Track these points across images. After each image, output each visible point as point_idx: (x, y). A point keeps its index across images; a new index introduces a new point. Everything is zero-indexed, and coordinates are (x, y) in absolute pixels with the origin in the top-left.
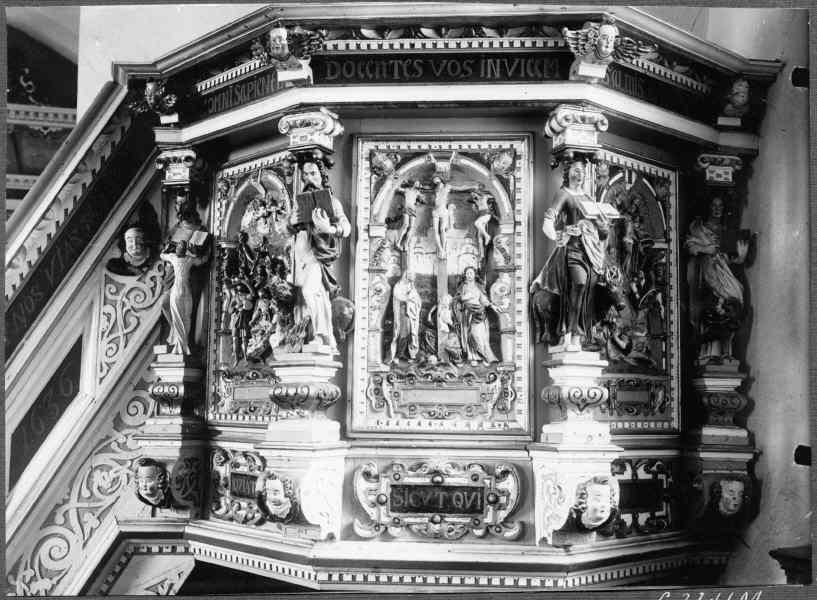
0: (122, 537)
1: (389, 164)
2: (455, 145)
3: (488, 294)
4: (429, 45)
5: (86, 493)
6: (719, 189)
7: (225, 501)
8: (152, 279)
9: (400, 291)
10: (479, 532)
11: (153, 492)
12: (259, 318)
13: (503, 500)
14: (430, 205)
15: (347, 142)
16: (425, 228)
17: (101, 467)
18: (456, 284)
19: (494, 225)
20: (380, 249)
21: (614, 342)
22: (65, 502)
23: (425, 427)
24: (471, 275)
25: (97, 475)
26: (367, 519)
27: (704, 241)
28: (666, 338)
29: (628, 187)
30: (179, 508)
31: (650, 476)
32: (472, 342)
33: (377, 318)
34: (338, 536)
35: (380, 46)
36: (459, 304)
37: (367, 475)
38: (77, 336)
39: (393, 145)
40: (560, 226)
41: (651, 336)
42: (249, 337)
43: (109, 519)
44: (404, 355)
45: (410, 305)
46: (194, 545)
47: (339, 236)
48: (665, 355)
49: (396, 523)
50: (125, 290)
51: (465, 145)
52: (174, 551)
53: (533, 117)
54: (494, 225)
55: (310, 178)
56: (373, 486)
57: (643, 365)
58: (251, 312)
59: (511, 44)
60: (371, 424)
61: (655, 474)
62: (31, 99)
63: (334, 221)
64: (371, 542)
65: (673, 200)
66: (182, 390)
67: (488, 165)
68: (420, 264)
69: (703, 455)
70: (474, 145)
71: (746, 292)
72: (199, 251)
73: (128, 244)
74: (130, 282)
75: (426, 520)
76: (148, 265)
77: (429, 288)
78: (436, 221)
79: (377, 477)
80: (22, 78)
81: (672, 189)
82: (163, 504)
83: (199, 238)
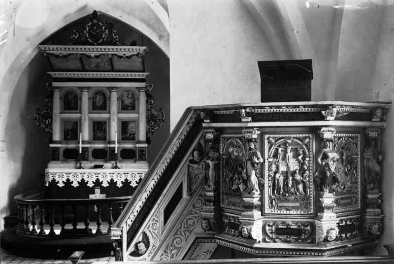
0: (197, 238)
1: (273, 141)
2: (292, 136)
3: (302, 177)
4: (284, 110)
5: (186, 226)
6: (375, 139)
7: (227, 229)
8: (202, 165)
9: (277, 176)
10: (300, 241)
11: (207, 227)
12: (236, 179)
13: (307, 232)
14: (285, 152)
15: (261, 136)
16: (284, 158)
17: (190, 219)
18: (294, 173)
19: (304, 159)
20: (271, 164)
21: (340, 187)
22: (180, 228)
23: (285, 212)
24: (297, 171)
25: (189, 221)
26: (269, 237)
27: (369, 154)
28: (356, 183)
29: (344, 142)
30: (214, 231)
31: (351, 223)
32: (298, 189)
33: (271, 183)
34: (261, 241)
35: (270, 111)
36: (294, 180)
37: (269, 226)
38: (180, 183)
39: (274, 135)
40: (322, 159)
41: (352, 183)
42: (233, 184)
43: (193, 233)
44: (279, 193)
45: (280, 180)
46: (217, 241)
47: (260, 162)
48: (356, 188)
49: (277, 238)
50: (194, 169)
51: (295, 136)
52: (211, 242)
53: (315, 130)
54: (304, 159)
55: (251, 147)
56: (270, 228)
57: (349, 192)
58: (233, 177)
59: (308, 110)
60: (270, 212)
61: (352, 222)
62: (118, 43)
63: (258, 159)
64: (270, 243)
65: (359, 143)
66: (213, 198)
67: (302, 141)
68: (283, 168)
69: (367, 217)
70: (298, 136)
71: (382, 170)
72: (218, 159)
73: (195, 155)
74: (196, 166)
75: (285, 237)
76: (201, 160)
77: (286, 175)
78: (287, 157)
79: (272, 226)
80: (113, 35)
81: (359, 139)
82: (209, 230)
83: (216, 155)
